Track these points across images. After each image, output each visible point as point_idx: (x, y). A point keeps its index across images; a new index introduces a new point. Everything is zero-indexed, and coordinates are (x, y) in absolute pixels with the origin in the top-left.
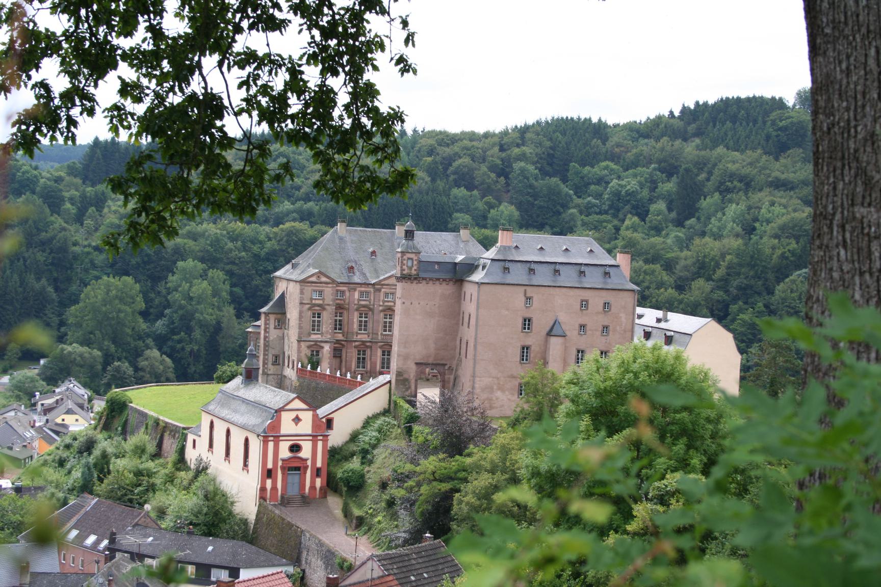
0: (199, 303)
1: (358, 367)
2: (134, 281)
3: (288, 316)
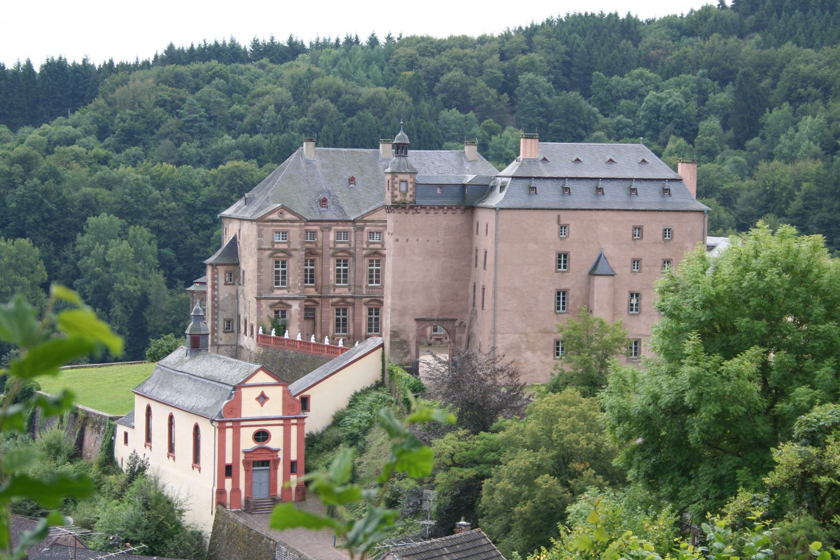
0: (118, 270)
1: (338, 331)
2: (32, 244)
3: (243, 267)
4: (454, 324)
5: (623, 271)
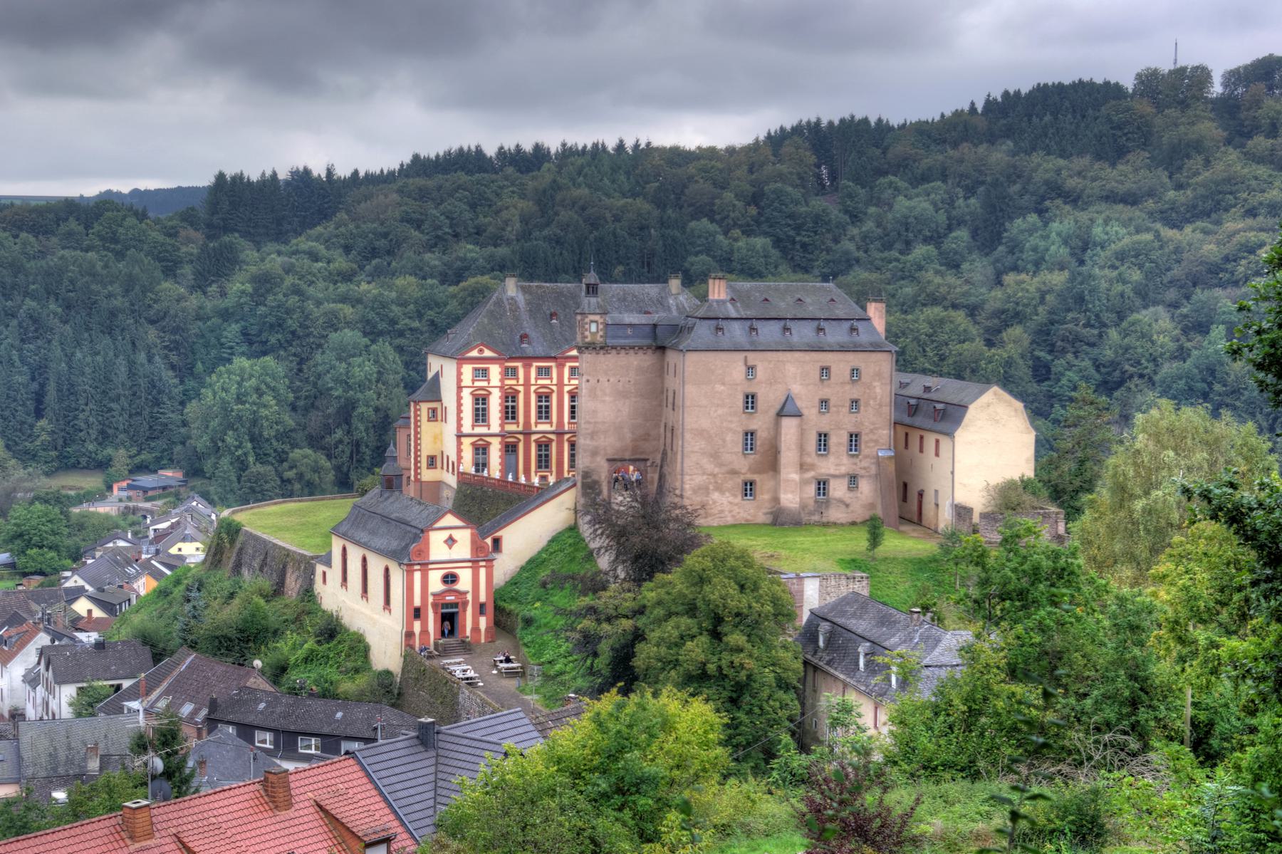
5: (811, 412)
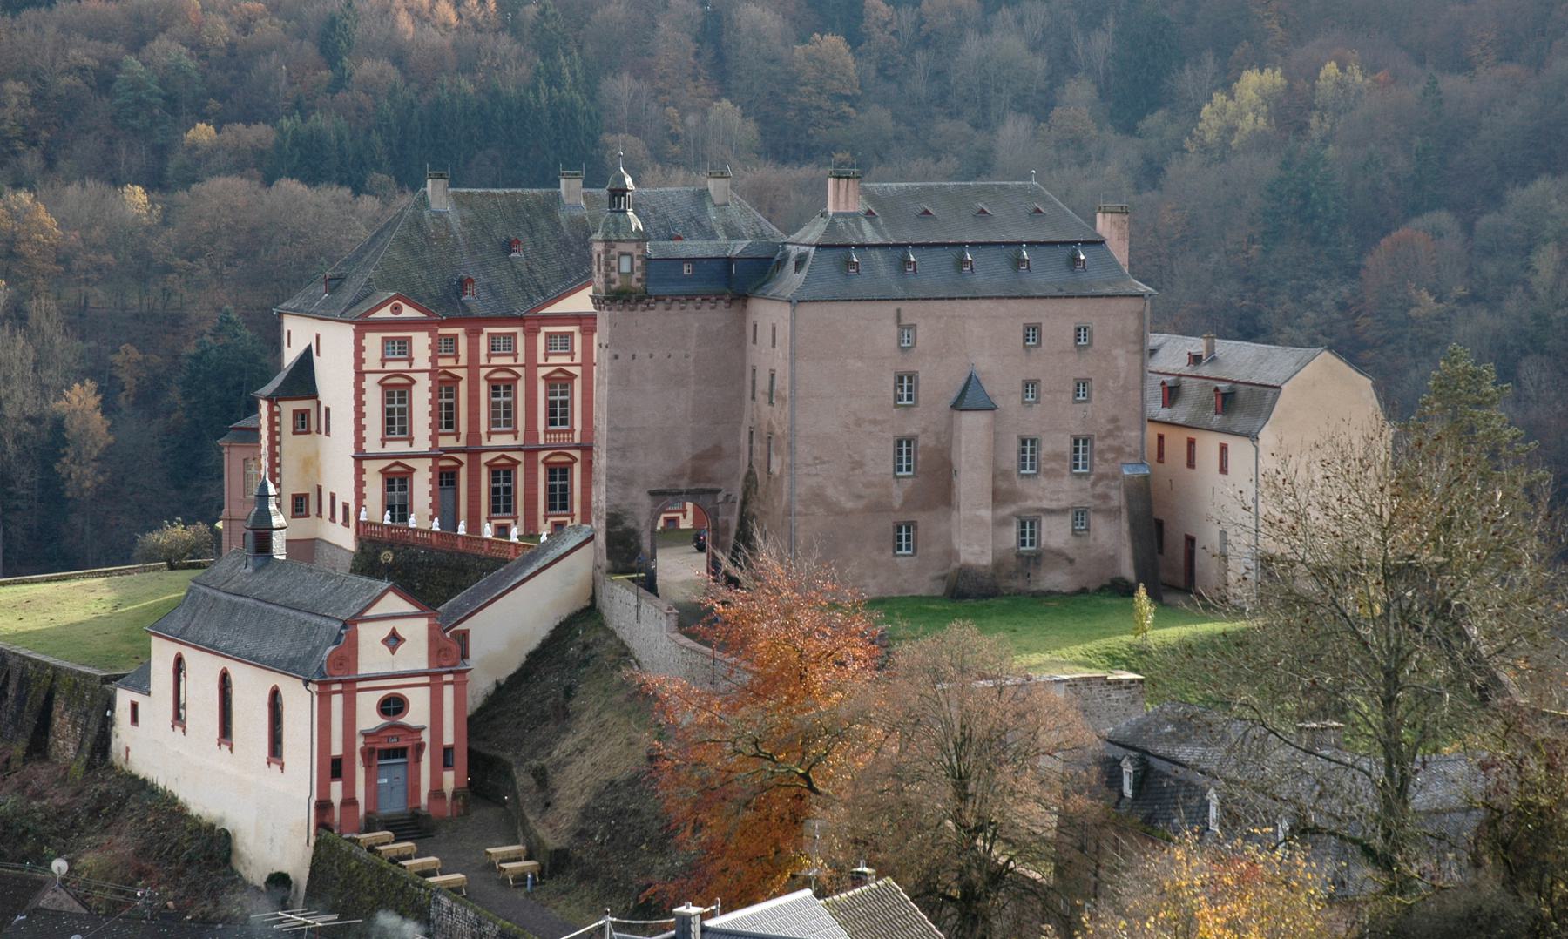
4: (716, 498)
